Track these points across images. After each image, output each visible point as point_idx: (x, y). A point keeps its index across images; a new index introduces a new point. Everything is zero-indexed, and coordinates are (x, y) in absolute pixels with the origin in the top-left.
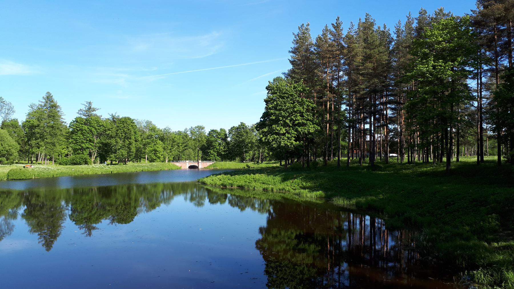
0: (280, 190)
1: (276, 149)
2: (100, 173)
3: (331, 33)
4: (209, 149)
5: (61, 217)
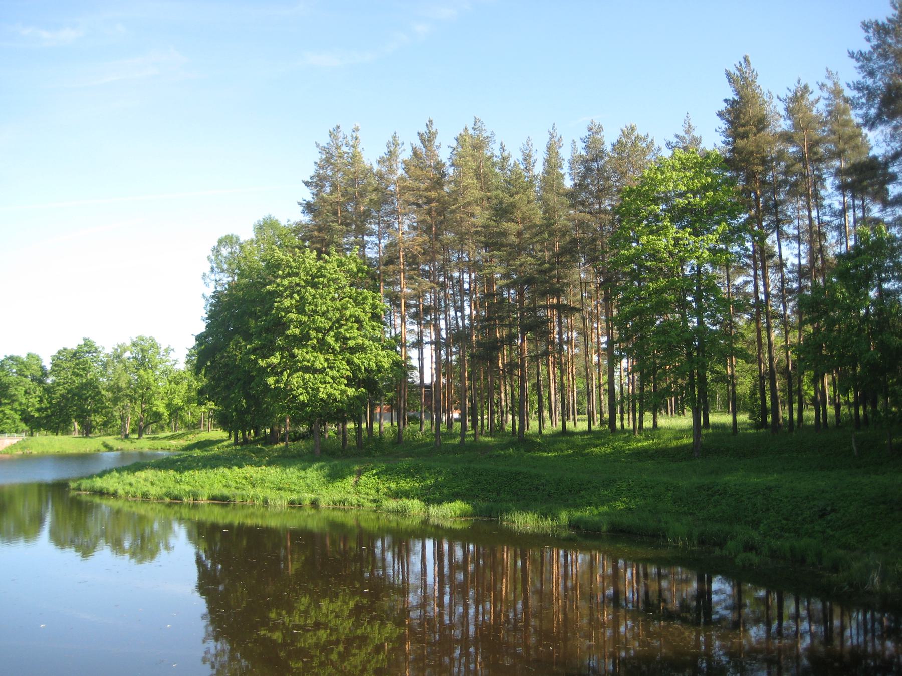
0: (334, 503)
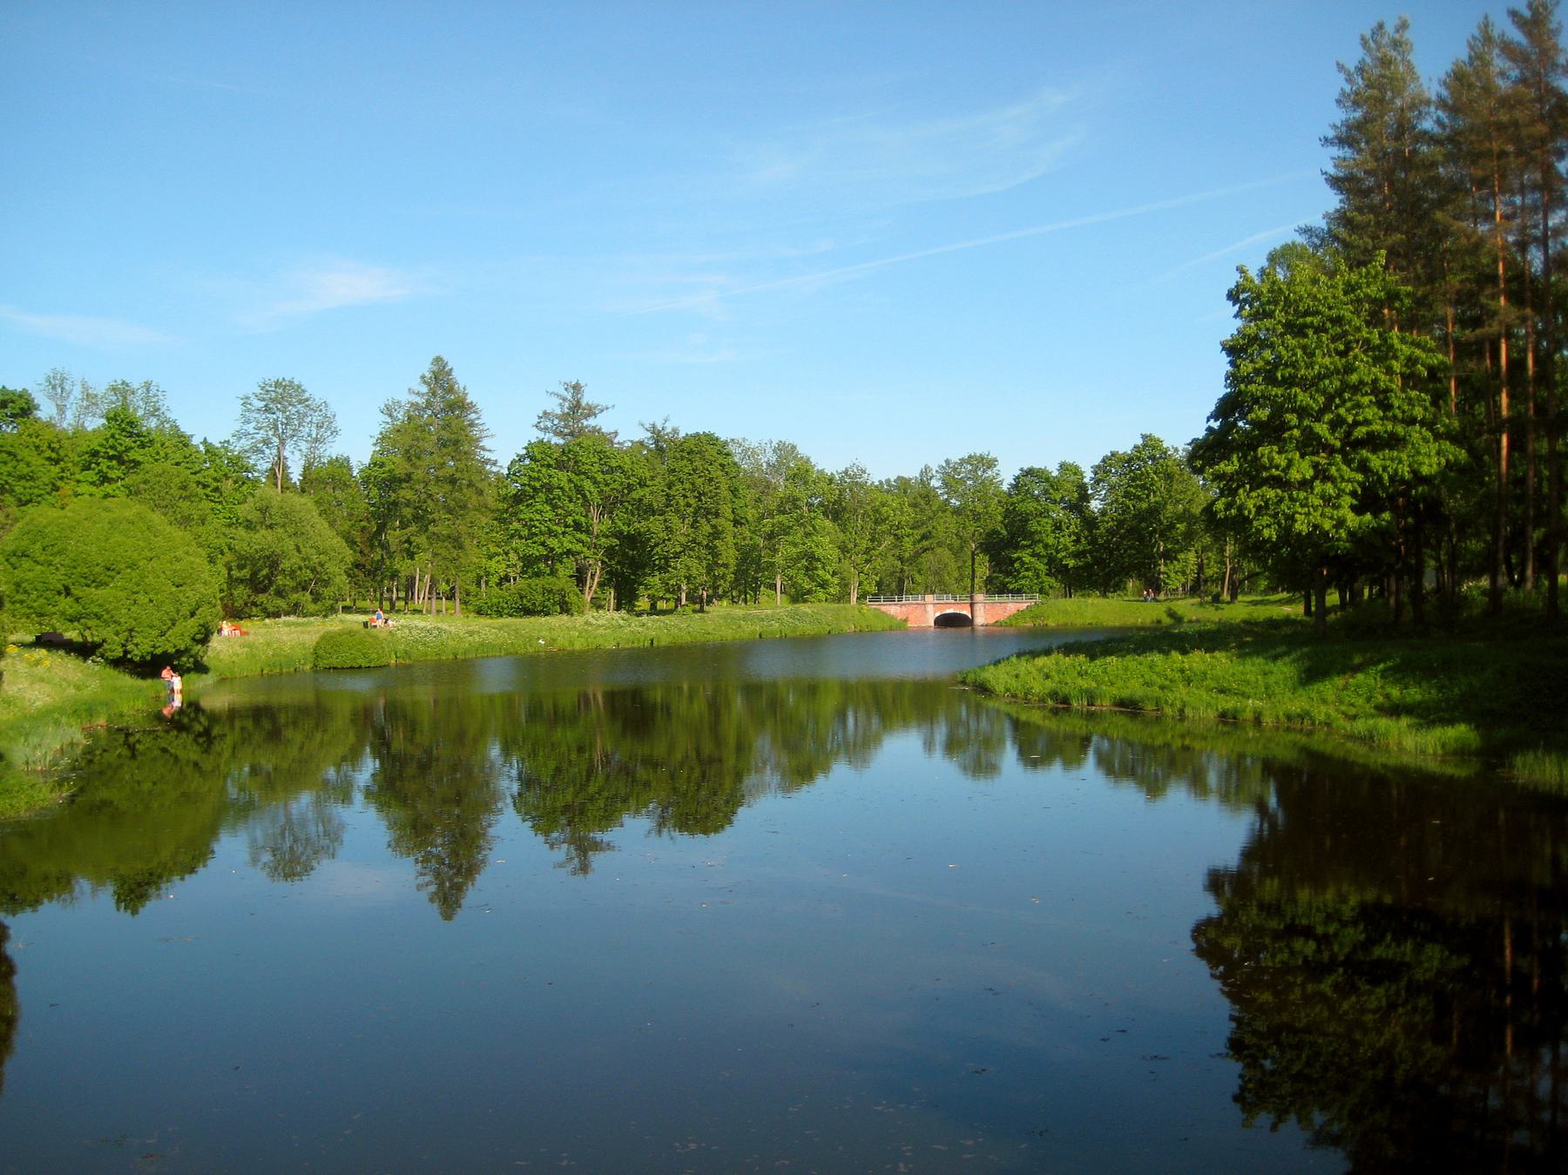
0: (1289, 718)
1: (1276, 547)
2: (611, 646)
3: (1508, 49)
4: (1017, 547)
5: (487, 805)
